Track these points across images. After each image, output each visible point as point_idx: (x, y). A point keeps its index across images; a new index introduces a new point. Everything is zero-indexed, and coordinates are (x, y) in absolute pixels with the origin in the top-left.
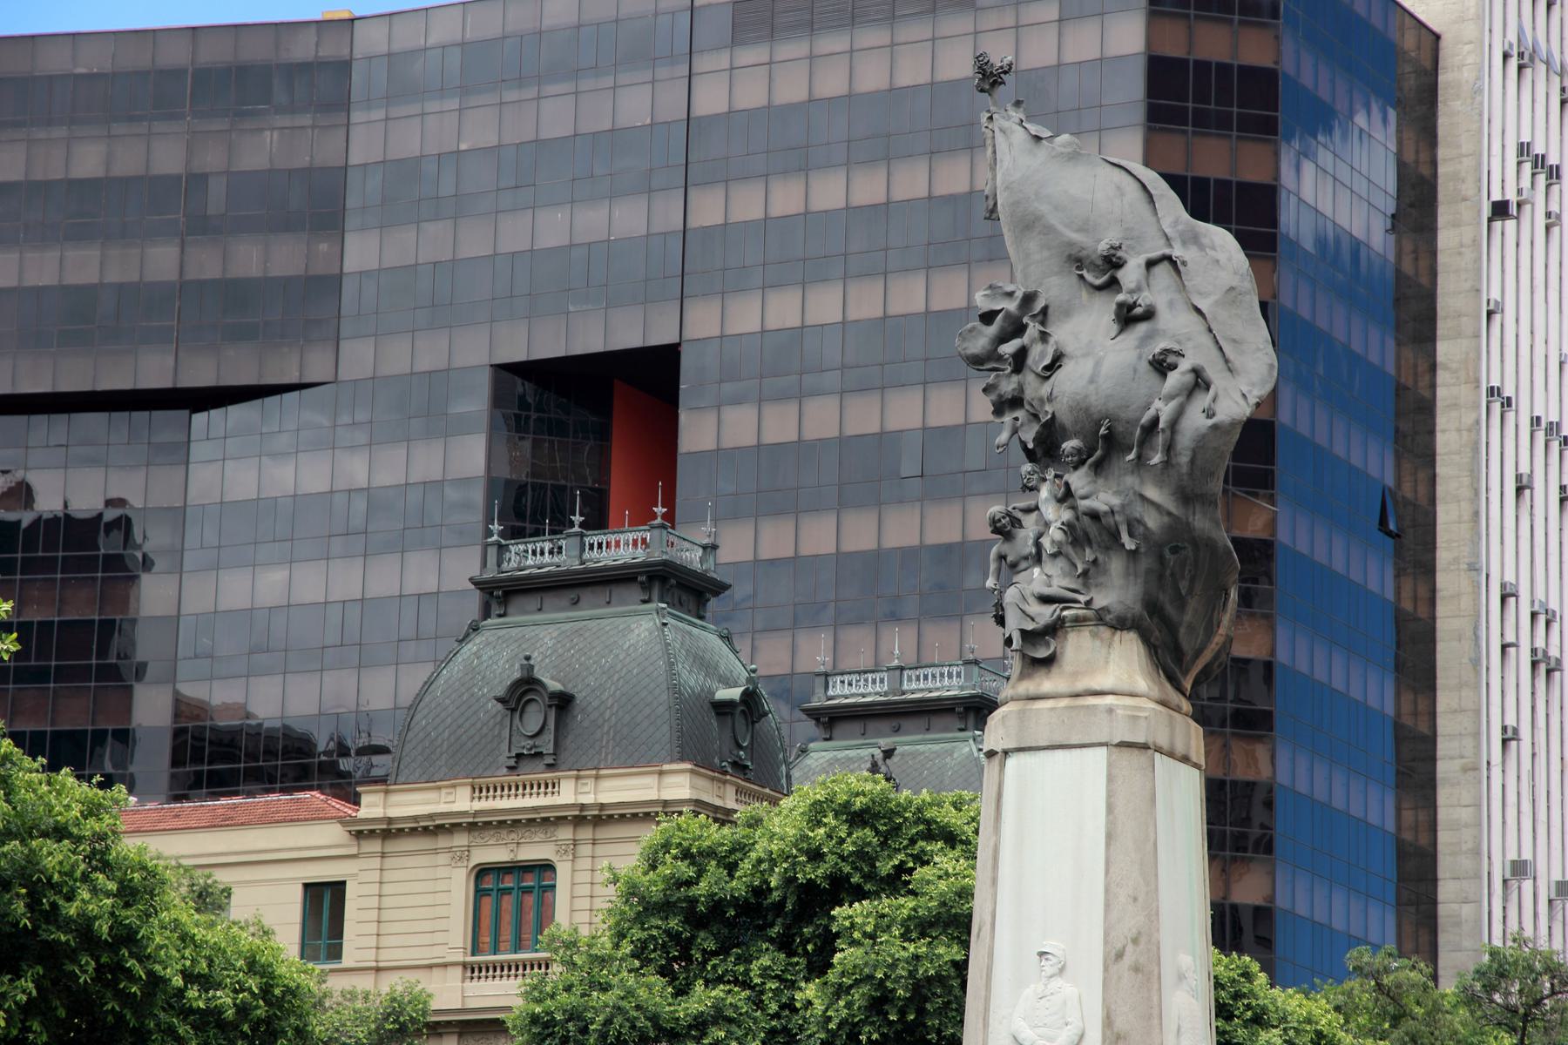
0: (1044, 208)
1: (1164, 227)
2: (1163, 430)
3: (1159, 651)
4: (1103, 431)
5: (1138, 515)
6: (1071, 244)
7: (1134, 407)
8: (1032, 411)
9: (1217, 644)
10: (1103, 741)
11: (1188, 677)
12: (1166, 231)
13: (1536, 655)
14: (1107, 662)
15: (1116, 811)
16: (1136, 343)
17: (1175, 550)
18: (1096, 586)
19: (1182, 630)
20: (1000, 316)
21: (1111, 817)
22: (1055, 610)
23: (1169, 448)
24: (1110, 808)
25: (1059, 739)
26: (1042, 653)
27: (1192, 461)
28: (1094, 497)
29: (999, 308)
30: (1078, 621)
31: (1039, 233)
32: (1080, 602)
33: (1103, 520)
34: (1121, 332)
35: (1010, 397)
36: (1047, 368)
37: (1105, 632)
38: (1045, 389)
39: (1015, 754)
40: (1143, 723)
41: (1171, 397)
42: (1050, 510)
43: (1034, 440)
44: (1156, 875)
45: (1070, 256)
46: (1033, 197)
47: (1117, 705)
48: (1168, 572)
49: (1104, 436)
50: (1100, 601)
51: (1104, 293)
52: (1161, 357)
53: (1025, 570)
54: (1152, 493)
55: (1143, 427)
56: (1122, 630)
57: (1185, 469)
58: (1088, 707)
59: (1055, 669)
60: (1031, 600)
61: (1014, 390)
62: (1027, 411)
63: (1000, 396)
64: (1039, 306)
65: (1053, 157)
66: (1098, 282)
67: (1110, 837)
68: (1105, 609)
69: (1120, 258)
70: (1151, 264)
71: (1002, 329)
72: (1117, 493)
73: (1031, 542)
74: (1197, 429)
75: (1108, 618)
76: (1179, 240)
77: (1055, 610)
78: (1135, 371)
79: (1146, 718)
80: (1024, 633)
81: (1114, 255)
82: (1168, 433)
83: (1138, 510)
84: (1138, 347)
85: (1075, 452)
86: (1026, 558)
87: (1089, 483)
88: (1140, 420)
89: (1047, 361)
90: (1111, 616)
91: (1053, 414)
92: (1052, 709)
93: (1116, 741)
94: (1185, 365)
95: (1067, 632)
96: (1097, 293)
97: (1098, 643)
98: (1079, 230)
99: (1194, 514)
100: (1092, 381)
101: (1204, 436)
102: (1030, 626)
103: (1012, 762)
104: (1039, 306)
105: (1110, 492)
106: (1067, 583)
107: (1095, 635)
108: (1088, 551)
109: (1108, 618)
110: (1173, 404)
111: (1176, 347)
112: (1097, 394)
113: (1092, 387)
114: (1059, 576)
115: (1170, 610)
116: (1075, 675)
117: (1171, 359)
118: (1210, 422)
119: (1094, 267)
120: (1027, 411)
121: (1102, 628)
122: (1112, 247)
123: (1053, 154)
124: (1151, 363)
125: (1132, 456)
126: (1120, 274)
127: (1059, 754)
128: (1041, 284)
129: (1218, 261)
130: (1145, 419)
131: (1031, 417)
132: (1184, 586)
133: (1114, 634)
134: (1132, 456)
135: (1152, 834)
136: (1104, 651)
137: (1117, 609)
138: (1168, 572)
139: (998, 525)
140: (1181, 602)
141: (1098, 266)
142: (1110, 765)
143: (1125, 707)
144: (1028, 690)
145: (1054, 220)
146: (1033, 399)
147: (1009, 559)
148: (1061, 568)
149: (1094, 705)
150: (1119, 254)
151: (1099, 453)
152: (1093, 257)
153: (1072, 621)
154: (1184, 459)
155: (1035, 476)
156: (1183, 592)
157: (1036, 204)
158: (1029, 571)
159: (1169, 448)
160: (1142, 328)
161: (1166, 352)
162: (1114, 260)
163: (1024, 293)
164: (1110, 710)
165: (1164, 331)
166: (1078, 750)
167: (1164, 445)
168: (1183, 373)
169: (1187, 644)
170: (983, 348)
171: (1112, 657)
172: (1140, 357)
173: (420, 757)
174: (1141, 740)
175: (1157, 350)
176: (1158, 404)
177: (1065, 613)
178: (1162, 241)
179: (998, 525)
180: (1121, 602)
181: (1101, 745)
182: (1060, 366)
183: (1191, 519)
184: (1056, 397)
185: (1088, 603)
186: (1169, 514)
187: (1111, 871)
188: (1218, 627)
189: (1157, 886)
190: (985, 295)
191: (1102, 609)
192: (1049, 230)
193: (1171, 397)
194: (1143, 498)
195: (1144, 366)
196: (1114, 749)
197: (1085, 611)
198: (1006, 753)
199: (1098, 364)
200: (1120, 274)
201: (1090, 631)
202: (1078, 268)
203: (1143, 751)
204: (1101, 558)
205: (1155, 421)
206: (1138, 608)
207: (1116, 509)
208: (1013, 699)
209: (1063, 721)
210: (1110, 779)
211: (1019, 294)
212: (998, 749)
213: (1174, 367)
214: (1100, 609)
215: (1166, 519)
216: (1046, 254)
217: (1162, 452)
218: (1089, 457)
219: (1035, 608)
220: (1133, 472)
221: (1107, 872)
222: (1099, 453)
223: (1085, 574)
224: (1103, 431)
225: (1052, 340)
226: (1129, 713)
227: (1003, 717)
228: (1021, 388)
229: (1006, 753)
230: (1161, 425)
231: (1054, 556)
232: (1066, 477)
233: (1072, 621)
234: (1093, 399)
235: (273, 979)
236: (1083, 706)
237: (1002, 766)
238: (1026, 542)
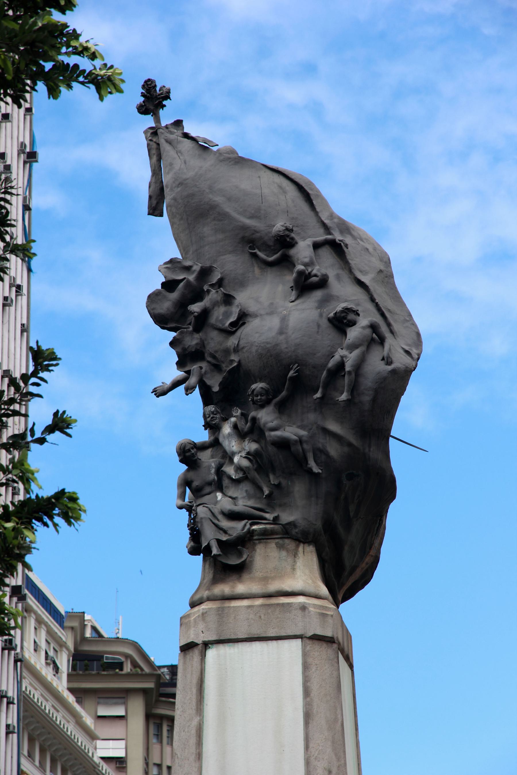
0: (218, 199)
1: (323, 219)
2: (349, 372)
3: (327, 565)
4: (291, 373)
5: (320, 446)
6: (244, 228)
7: (319, 355)
8: (213, 361)
9: (367, 564)
10: (298, 633)
11: (341, 591)
12: (326, 221)
13: (9, 729)
14: (294, 569)
15: (312, 695)
16: (316, 304)
17: (351, 477)
18: (280, 506)
19: (346, 548)
20: (182, 284)
21: (308, 699)
22: (245, 525)
23: (354, 389)
24: (307, 692)
25: (256, 631)
26: (234, 561)
27: (374, 400)
28: (282, 429)
29: (180, 277)
30: (266, 535)
31: (214, 219)
32: (265, 519)
33: (293, 449)
34: (298, 297)
35: (193, 350)
36: (232, 324)
37: (290, 544)
38: (232, 342)
39: (215, 645)
40: (330, 620)
41: (352, 347)
42: (233, 443)
43: (220, 385)
44: (344, 752)
45: (243, 238)
46: (207, 191)
47: (309, 604)
48: (343, 496)
49: (291, 378)
50: (286, 517)
51: (274, 269)
52: (343, 315)
53: (209, 494)
54: (334, 427)
55: (329, 371)
56: (304, 543)
57: (367, 407)
58: (283, 605)
59: (245, 576)
60: (220, 517)
61: (197, 344)
62: (208, 362)
63: (184, 349)
64: (215, 278)
65: (221, 161)
66: (271, 259)
67: (308, 717)
68: (292, 524)
69: (293, 239)
70: (316, 246)
71: (183, 295)
72: (302, 427)
73: (213, 471)
74: (379, 373)
75: (294, 531)
76: (337, 230)
77: (245, 525)
78: (319, 326)
79: (332, 616)
80: (220, 542)
81: (288, 236)
82: (353, 375)
83: (322, 441)
84: (317, 308)
85: (264, 392)
86: (210, 484)
87: (277, 418)
88: (327, 364)
89: (233, 318)
90: (297, 530)
91: (239, 362)
92: (249, 607)
93: (310, 634)
94: (363, 321)
95: (255, 545)
96: (269, 269)
97: (284, 553)
98: (252, 217)
99: (370, 447)
100: (281, 332)
101: (385, 379)
102: (224, 538)
103: (211, 653)
104: (215, 278)
105: (294, 426)
106: (251, 503)
107: (280, 547)
108: (271, 477)
109: (294, 531)
110: (356, 353)
111: (355, 308)
112: (287, 342)
113: (282, 337)
114: (243, 498)
115: (341, 530)
116: (265, 579)
117: (351, 316)
118: (390, 368)
119: (266, 247)
120: (208, 362)
121: (287, 541)
122: (287, 229)
123: (222, 158)
124: (330, 320)
125: (318, 395)
126: (292, 252)
127: (257, 646)
128: (215, 261)
129: (367, 249)
130: (331, 364)
131: (212, 368)
132: (352, 508)
133: (298, 546)
134: (318, 395)
135: (339, 716)
136: (290, 560)
137: (302, 524)
138: (343, 496)
139: (188, 454)
140: (348, 524)
141: (269, 246)
142: (305, 655)
143: (315, 606)
144: (223, 591)
145: (228, 208)
146: (216, 352)
147: (195, 484)
148: (246, 491)
149: (288, 604)
150: (293, 235)
151: (284, 393)
152: (266, 238)
153: (259, 535)
154: (366, 398)
155: (218, 416)
156: (352, 514)
157: (211, 196)
158: (212, 495)
159: (354, 389)
160: (318, 294)
161: (347, 310)
162: (288, 240)
163: (201, 267)
164: (303, 608)
165: (338, 297)
166: (274, 643)
167: (349, 385)
168: (364, 328)
169: (348, 560)
170: (168, 309)
171: (298, 564)
172: (321, 315)
173: (15, 426)
174: (329, 634)
175: (339, 308)
176: (344, 352)
177: (255, 527)
178: (322, 231)
179: (188, 454)
180: (305, 519)
181: (295, 637)
182: (244, 324)
183: (367, 450)
184: (243, 348)
185: (276, 520)
186: (350, 445)
187: (311, 745)
188: (370, 548)
189: (345, 761)
190: (167, 268)
191: (289, 524)
192: (223, 216)
193: (352, 347)
194: (326, 431)
195: (325, 323)
196: (308, 641)
197: (272, 526)
198: (206, 645)
199: (284, 320)
200: (292, 252)
201: (277, 544)
202: (250, 248)
203: (330, 644)
204: (284, 482)
205: (341, 365)
206: (319, 525)
207: (304, 439)
208: (209, 599)
209: (260, 617)
210: (306, 667)
211: (197, 268)
212: (199, 641)
213: (353, 323)
214: (287, 524)
215: (346, 449)
216: (220, 236)
217: (348, 391)
218: (275, 397)
219: (225, 523)
220: (315, 410)
221: (307, 747)
222: (284, 393)
223: (269, 496)
224: (291, 373)
225: (236, 302)
226: (318, 611)
227: (203, 614)
228: (202, 344)
229: (206, 645)
230: (348, 368)
231: (237, 482)
232: (253, 414)
233: (259, 535)
234: (283, 346)
235: (192, 661)
236: (278, 605)
237: (203, 656)
238: (209, 470)
